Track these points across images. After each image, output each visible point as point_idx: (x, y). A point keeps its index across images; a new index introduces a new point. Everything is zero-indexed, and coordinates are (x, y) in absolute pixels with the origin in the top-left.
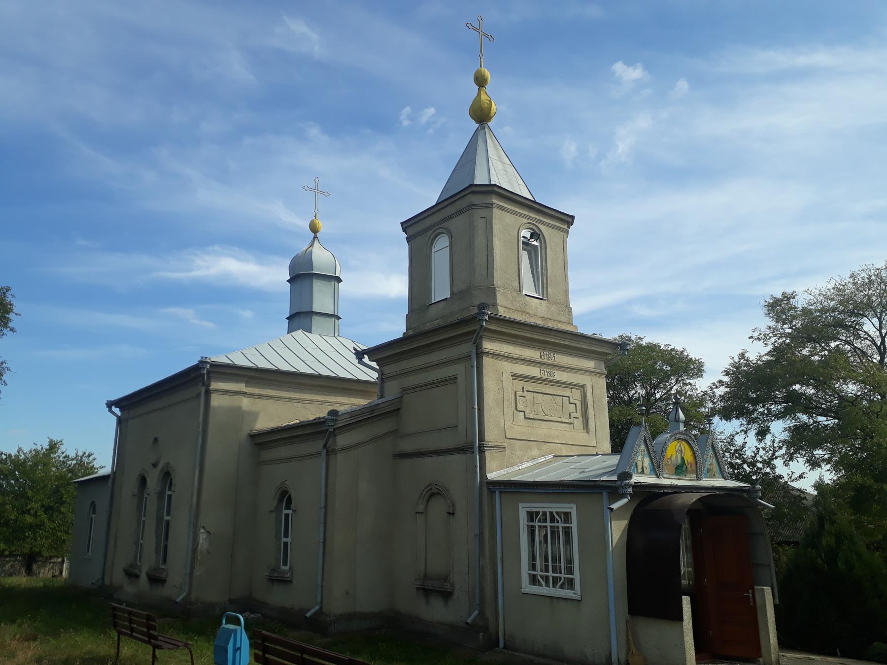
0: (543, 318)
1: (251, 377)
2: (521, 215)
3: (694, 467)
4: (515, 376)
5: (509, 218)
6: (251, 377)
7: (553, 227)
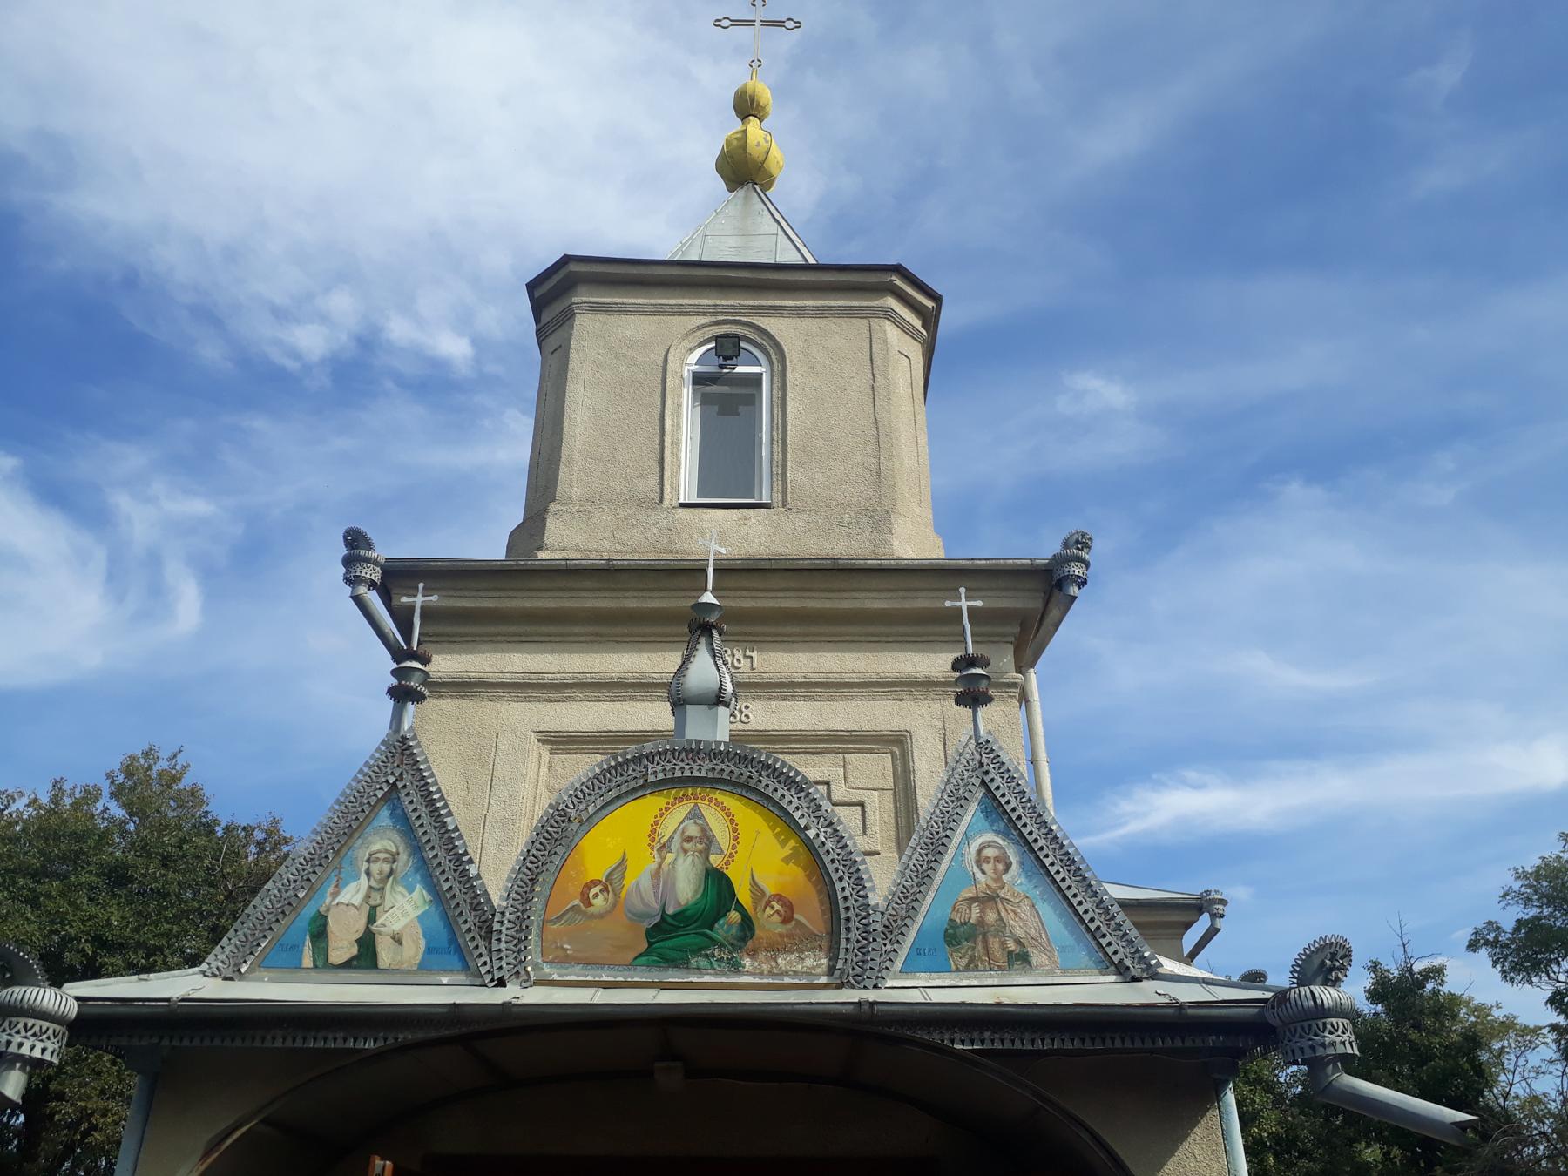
2: (681, 311)
3: (811, 916)
5: (633, 328)
7: (800, 313)
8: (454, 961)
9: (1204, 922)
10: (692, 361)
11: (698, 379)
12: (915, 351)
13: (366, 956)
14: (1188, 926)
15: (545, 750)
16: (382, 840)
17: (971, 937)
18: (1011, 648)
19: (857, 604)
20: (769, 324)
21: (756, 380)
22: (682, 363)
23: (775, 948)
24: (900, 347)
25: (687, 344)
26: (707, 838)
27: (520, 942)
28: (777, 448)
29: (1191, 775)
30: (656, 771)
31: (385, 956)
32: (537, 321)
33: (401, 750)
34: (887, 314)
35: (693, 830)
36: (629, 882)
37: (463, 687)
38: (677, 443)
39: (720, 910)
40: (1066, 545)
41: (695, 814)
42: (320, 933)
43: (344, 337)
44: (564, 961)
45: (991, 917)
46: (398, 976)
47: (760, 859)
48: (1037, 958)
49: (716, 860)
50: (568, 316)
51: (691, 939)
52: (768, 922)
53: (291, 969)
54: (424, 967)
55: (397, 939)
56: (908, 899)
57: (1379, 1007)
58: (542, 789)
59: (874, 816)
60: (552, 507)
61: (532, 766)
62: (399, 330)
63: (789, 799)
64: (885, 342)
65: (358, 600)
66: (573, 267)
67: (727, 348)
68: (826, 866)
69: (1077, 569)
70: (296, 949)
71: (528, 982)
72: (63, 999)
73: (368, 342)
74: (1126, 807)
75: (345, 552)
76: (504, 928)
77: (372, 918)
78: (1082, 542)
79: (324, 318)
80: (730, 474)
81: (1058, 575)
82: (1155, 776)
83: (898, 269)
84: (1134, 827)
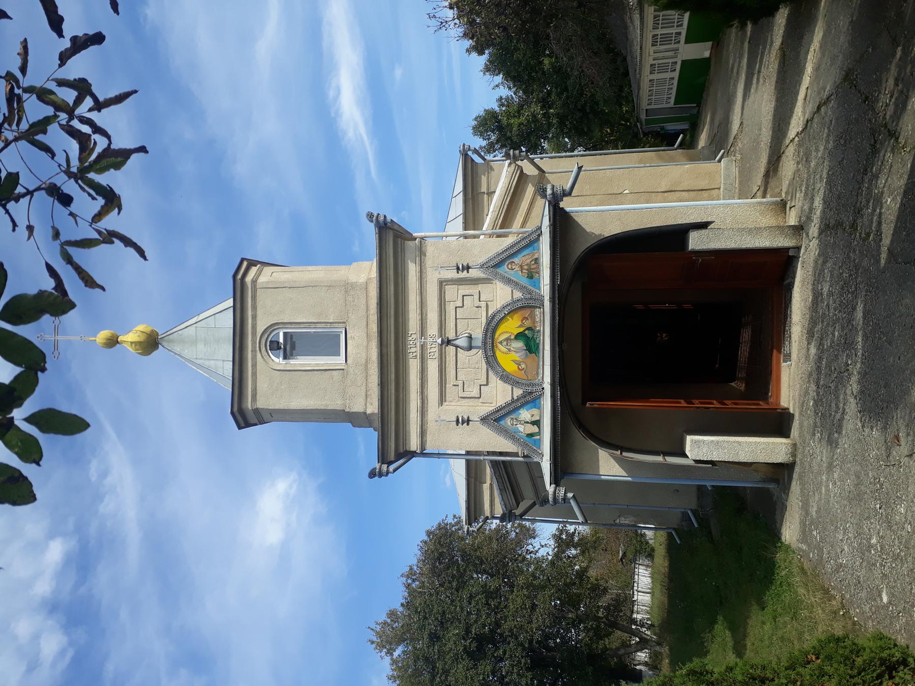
0: (368, 336)
1: (476, 479)
2: (254, 365)
3: (526, 313)
4: (442, 399)
5: (263, 385)
6: (476, 479)
7: (254, 317)
8: (537, 401)
9: (470, 153)
10: (278, 361)
11: (285, 358)
12: (268, 270)
13: (537, 423)
14: (472, 160)
15: (445, 404)
16: (508, 422)
17: (531, 273)
18: (407, 242)
19: (392, 297)
20: (260, 329)
21: (285, 334)
22: (279, 364)
23: (534, 322)
24: (267, 276)
25: (271, 362)
26: (507, 339)
27: (533, 385)
28: (319, 326)
29: (331, 94)
30: (490, 353)
31: (537, 418)
32: (256, 425)
33: (484, 420)
34: (254, 282)
35: (505, 343)
36: (518, 359)
37: (423, 433)
38: (317, 365)
39: (525, 336)
40: (372, 221)
41: (501, 343)
42: (530, 435)
43: (50, 622)
44: (537, 374)
45: (526, 267)
46: (541, 415)
47: (512, 326)
48: (536, 256)
49: (513, 337)
50: (257, 411)
51: (532, 343)
52: (528, 323)
53: (539, 443)
54: (539, 408)
55: (533, 416)
56: (522, 288)
57: (487, 52)
58: (458, 403)
59: (467, 292)
60: (347, 410)
61: (451, 407)
62: (43, 588)
63: (497, 318)
64: (268, 282)
65: (395, 471)
66: (236, 409)
67: (274, 346)
68: (513, 309)
69: (381, 218)
70: (535, 441)
71: (543, 382)
72: (550, 489)
73: (52, 607)
74: (351, 134)
75: (377, 478)
76: (530, 389)
77: (527, 422)
78: (370, 216)
79: (36, 637)
80: (326, 342)
81: (383, 225)
82: (333, 115)
83: (235, 276)
84: (362, 130)
